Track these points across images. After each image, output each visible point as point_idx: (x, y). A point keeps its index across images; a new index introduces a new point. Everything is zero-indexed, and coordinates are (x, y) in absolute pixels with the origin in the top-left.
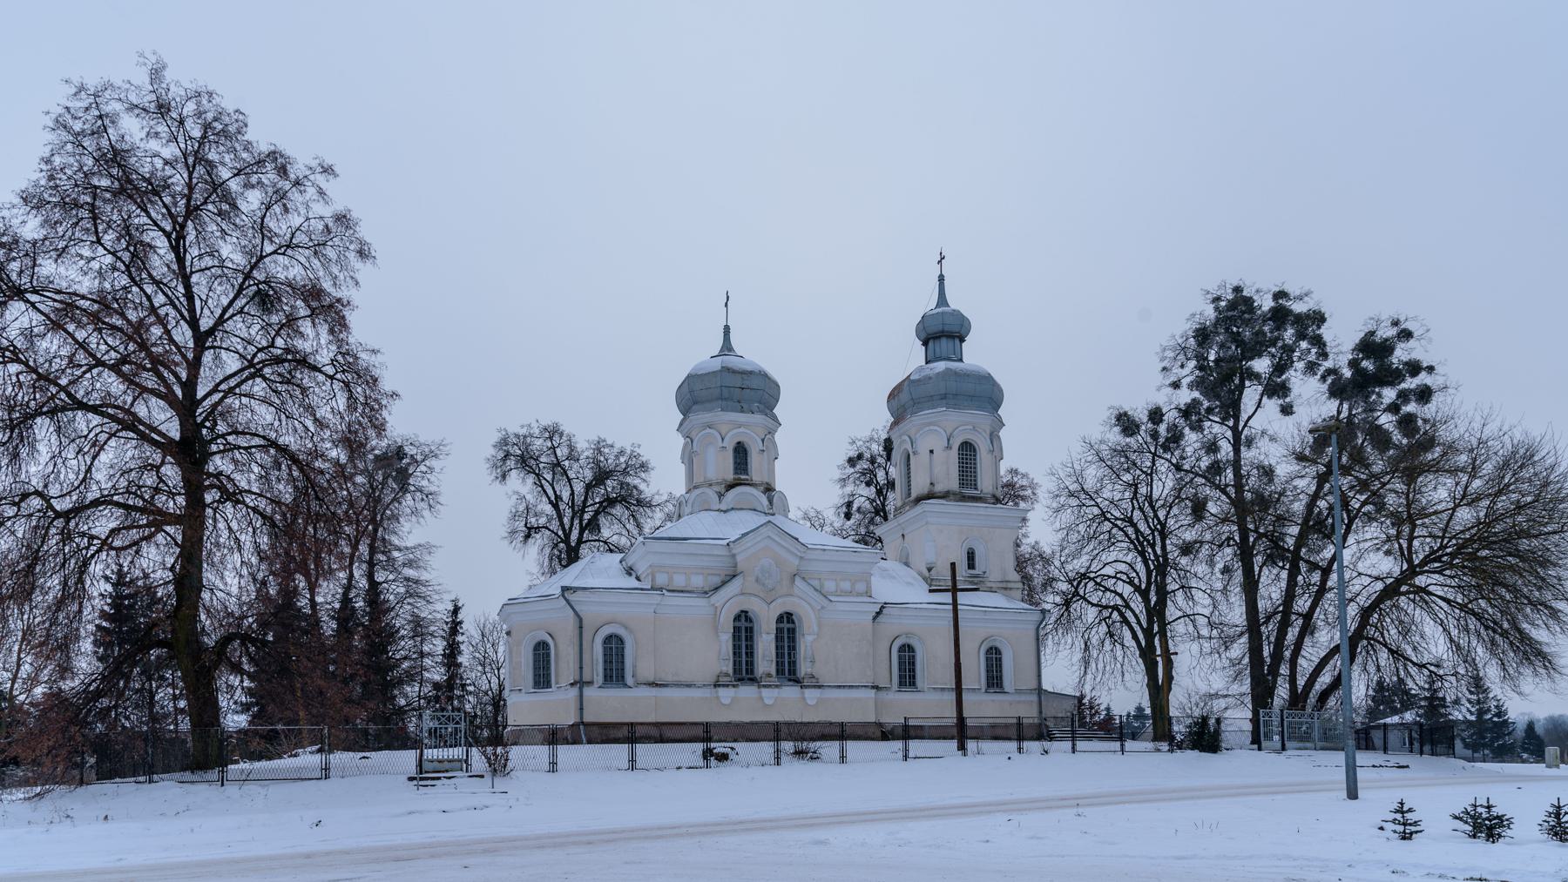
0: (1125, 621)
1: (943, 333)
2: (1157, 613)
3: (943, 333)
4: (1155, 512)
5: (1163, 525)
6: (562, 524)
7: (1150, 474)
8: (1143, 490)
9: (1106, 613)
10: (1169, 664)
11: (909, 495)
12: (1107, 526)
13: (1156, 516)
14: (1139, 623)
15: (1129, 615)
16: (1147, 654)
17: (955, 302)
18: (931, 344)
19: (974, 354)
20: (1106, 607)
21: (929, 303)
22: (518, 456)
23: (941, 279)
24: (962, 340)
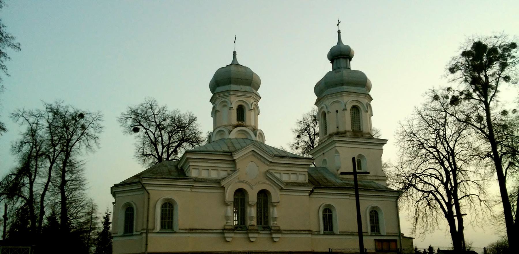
0: (437, 199)
1: (340, 56)
2: (452, 193)
3: (340, 56)
4: (448, 143)
5: (453, 151)
6: (158, 152)
7: (444, 125)
8: (441, 133)
9: (426, 195)
10: (461, 221)
11: (326, 133)
12: (424, 151)
13: (449, 146)
14: (444, 199)
15: (439, 196)
16: (449, 216)
17: (345, 42)
18: (335, 61)
19: (355, 65)
20: (425, 192)
21: (335, 43)
22: (139, 120)
23: (339, 32)
24: (350, 60)
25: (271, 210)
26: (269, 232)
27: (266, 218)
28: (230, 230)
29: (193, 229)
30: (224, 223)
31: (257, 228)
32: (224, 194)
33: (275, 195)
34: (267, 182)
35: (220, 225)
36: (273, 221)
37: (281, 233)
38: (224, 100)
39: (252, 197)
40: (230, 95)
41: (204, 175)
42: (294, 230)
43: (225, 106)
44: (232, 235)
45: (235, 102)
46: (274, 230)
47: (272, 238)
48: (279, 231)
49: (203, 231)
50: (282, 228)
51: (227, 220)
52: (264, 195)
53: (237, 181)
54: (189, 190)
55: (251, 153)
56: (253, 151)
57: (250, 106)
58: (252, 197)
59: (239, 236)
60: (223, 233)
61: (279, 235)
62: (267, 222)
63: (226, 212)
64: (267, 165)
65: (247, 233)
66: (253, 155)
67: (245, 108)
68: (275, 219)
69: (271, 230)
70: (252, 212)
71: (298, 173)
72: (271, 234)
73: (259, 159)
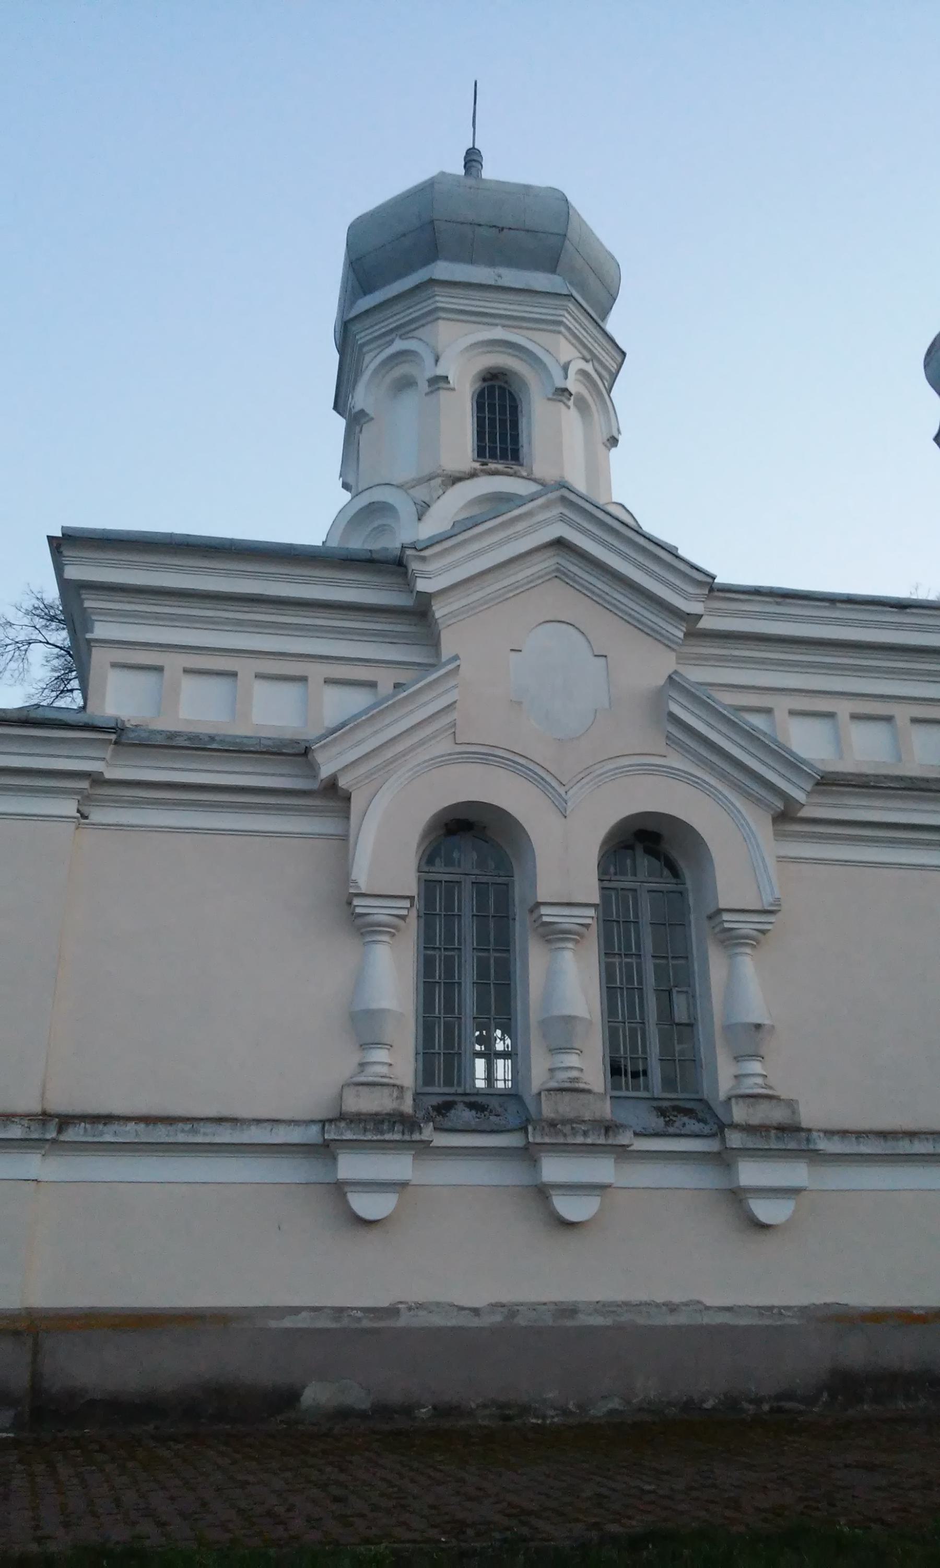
25: (716, 966)
26: (711, 1145)
27: (682, 1032)
28: (378, 1121)
29: (65, 1121)
30: (343, 1065)
31: (605, 1110)
32: (343, 842)
33: (741, 860)
34: (676, 761)
35: (301, 1078)
36: (737, 1059)
37: (815, 1157)
38: (399, 345)
39: (564, 865)
40: (432, 315)
41: (198, 707)
42: (912, 1135)
43: (406, 383)
44: (399, 1166)
45: (458, 352)
46: (749, 1129)
47: (737, 1197)
48: (788, 1137)
49: (164, 1132)
50: (808, 1116)
51: (365, 1046)
52: (648, 847)
53: (443, 746)
54: (69, 807)
55: (548, 562)
56: (560, 544)
57: (557, 373)
58: (564, 865)
59: (461, 1176)
60: (325, 1151)
61: (795, 1174)
62: (684, 1062)
63: (359, 979)
64: (666, 642)
65: (529, 1155)
66: (560, 574)
67: (524, 384)
68: (751, 1038)
69: (721, 1128)
70: (566, 982)
71: (902, 713)
72: (724, 1160)
73: (611, 608)
